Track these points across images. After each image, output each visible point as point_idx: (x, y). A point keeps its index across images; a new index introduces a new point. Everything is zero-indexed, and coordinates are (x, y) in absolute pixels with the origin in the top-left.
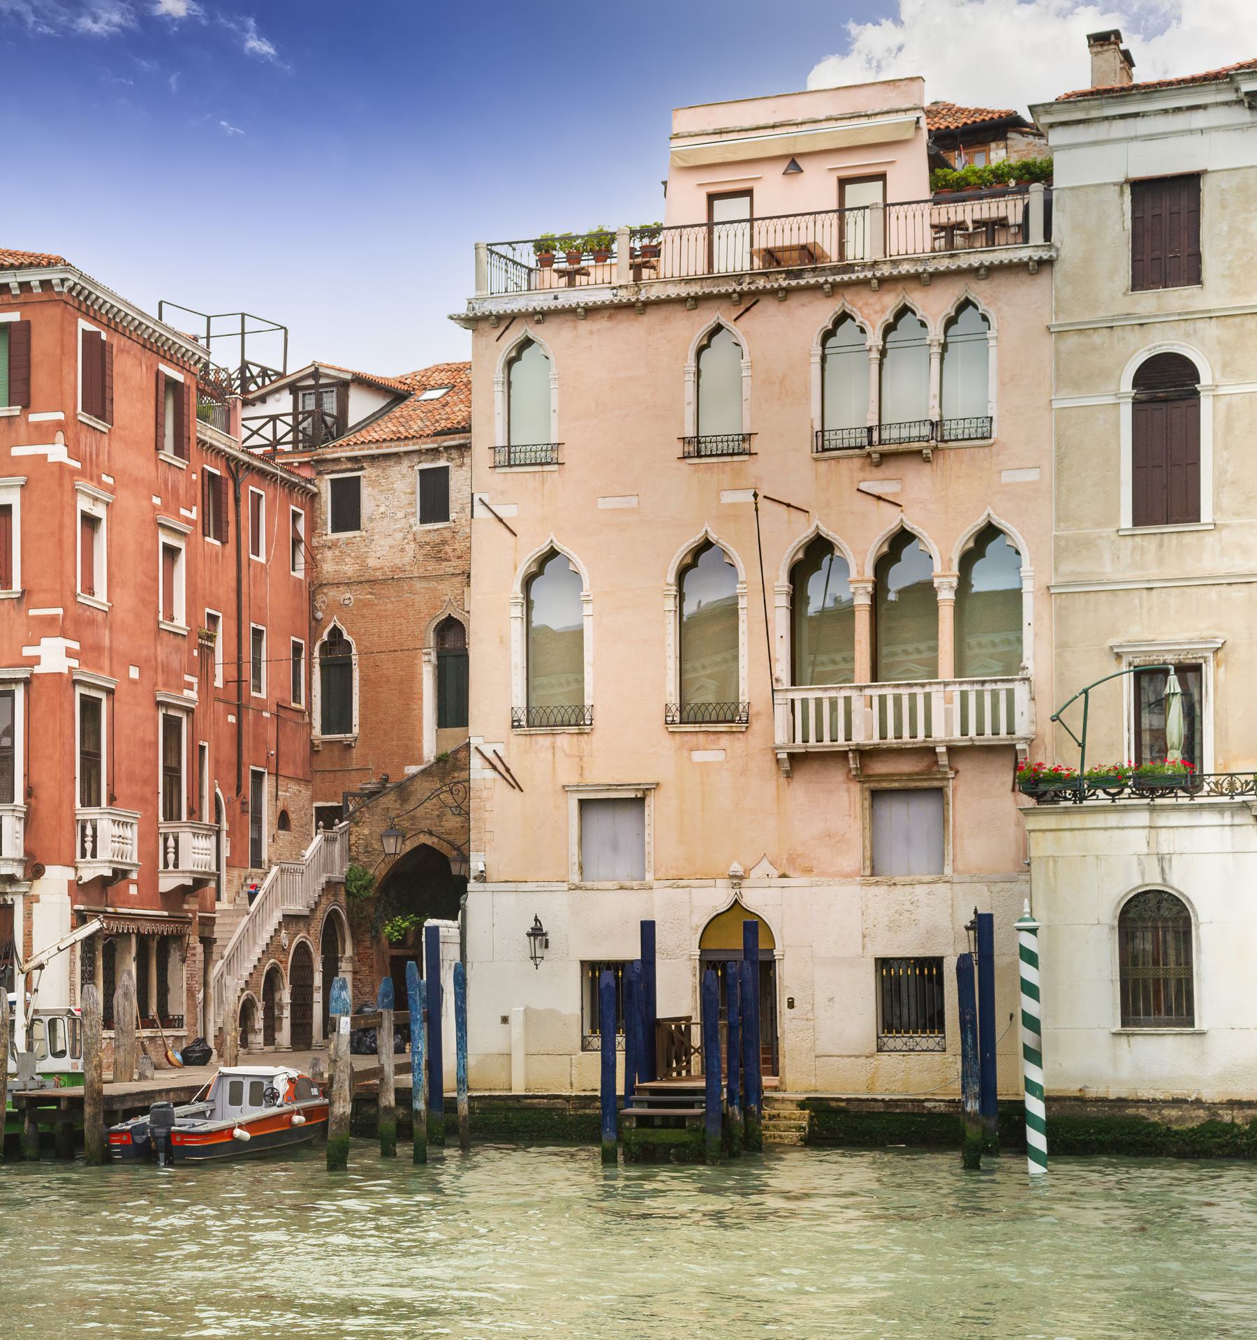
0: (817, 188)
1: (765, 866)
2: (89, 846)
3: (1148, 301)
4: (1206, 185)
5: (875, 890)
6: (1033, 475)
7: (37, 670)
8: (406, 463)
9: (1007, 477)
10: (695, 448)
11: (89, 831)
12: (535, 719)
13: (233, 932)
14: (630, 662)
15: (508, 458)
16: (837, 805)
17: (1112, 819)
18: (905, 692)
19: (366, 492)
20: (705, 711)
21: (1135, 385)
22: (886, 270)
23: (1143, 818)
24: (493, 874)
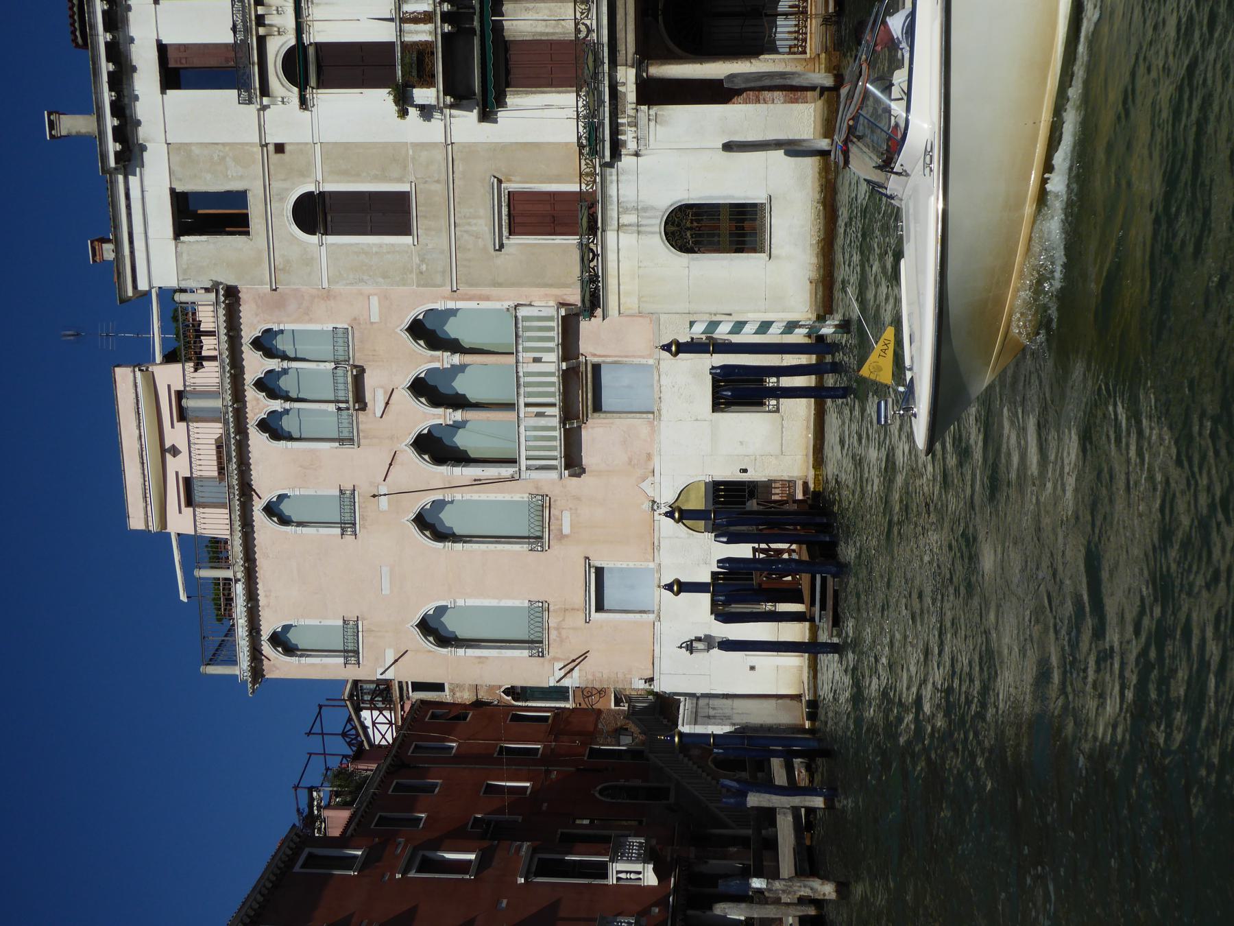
1: (645, 485)
3: (256, 222)
4: (180, 188)
5: (664, 412)
6: (375, 301)
9: (375, 318)
10: (348, 526)
12: (535, 644)
16: (595, 434)
17: (611, 256)
21: (313, 233)
23: (611, 236)
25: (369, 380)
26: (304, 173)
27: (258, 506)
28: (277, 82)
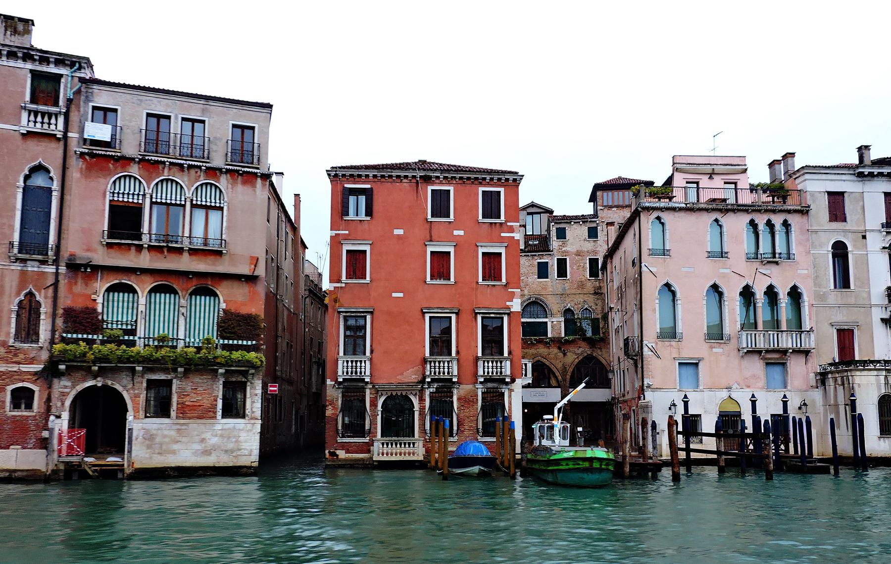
0: (718, 182)
6: (806, 272)
16: (756, 366)
22: (735, 207)
26: (854, 246)
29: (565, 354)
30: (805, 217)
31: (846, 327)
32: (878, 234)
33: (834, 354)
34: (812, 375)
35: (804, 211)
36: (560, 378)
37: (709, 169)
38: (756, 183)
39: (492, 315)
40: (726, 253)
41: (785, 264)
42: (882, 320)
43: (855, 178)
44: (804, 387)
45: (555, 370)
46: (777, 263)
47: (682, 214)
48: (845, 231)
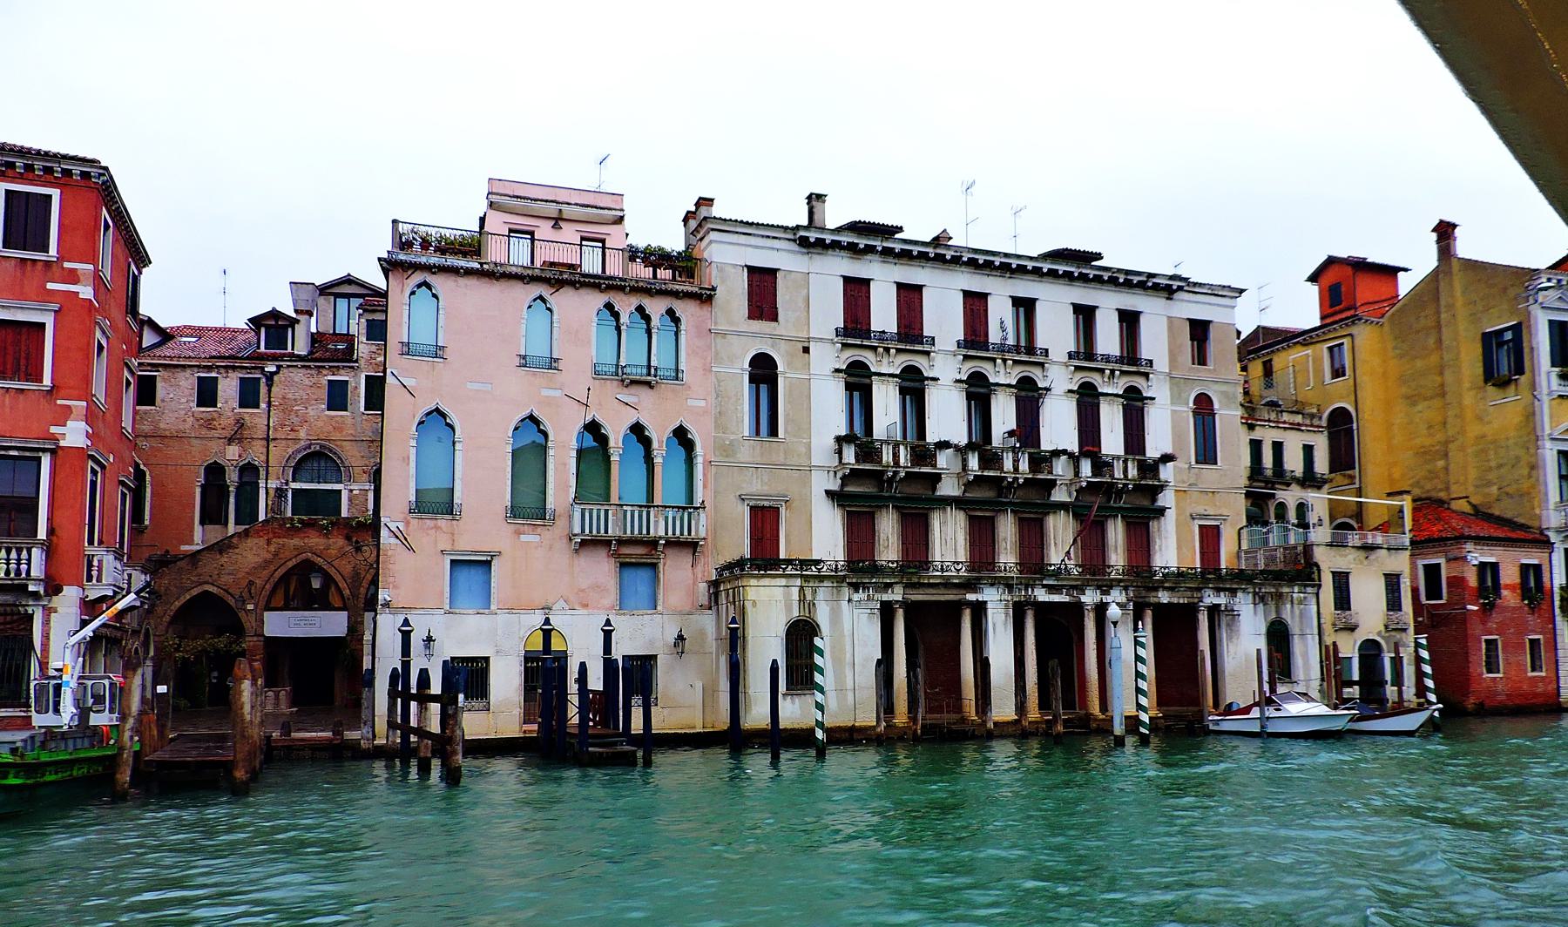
0: (570, 233)
1: (561, 603)
2: (95, 573)
6: (703, 403)
7: (62, 443)
8: (189, 371)
11: (95, 563)
13: (104, 625)
14: (483, 476)
15: (407, 349)
16: (601, 569)
18: (595, 508)
19: (159, 385)
20: (528, 508)
24: (394, 604)
25: (643, 392)
26: (789, 364)
27: (545, 291)
28: (970, 367)
29: (358, 549)
30: (706, 308)
31: (766, 504)
32: (829, 346)
33: (742, 547)
34: (703, 586)
35: (705, 297)
36: (347, 592)
37: (552, 210)
38: (642, 245)
39: (12, 453)
40: (556, 360)
41: (666, 389)
42: (827, 492)
43: (796, 248)
44: (687, 609)
45: (338, 578)
46: (648, 384)
47: (472, 282)
48: (772, 337)
